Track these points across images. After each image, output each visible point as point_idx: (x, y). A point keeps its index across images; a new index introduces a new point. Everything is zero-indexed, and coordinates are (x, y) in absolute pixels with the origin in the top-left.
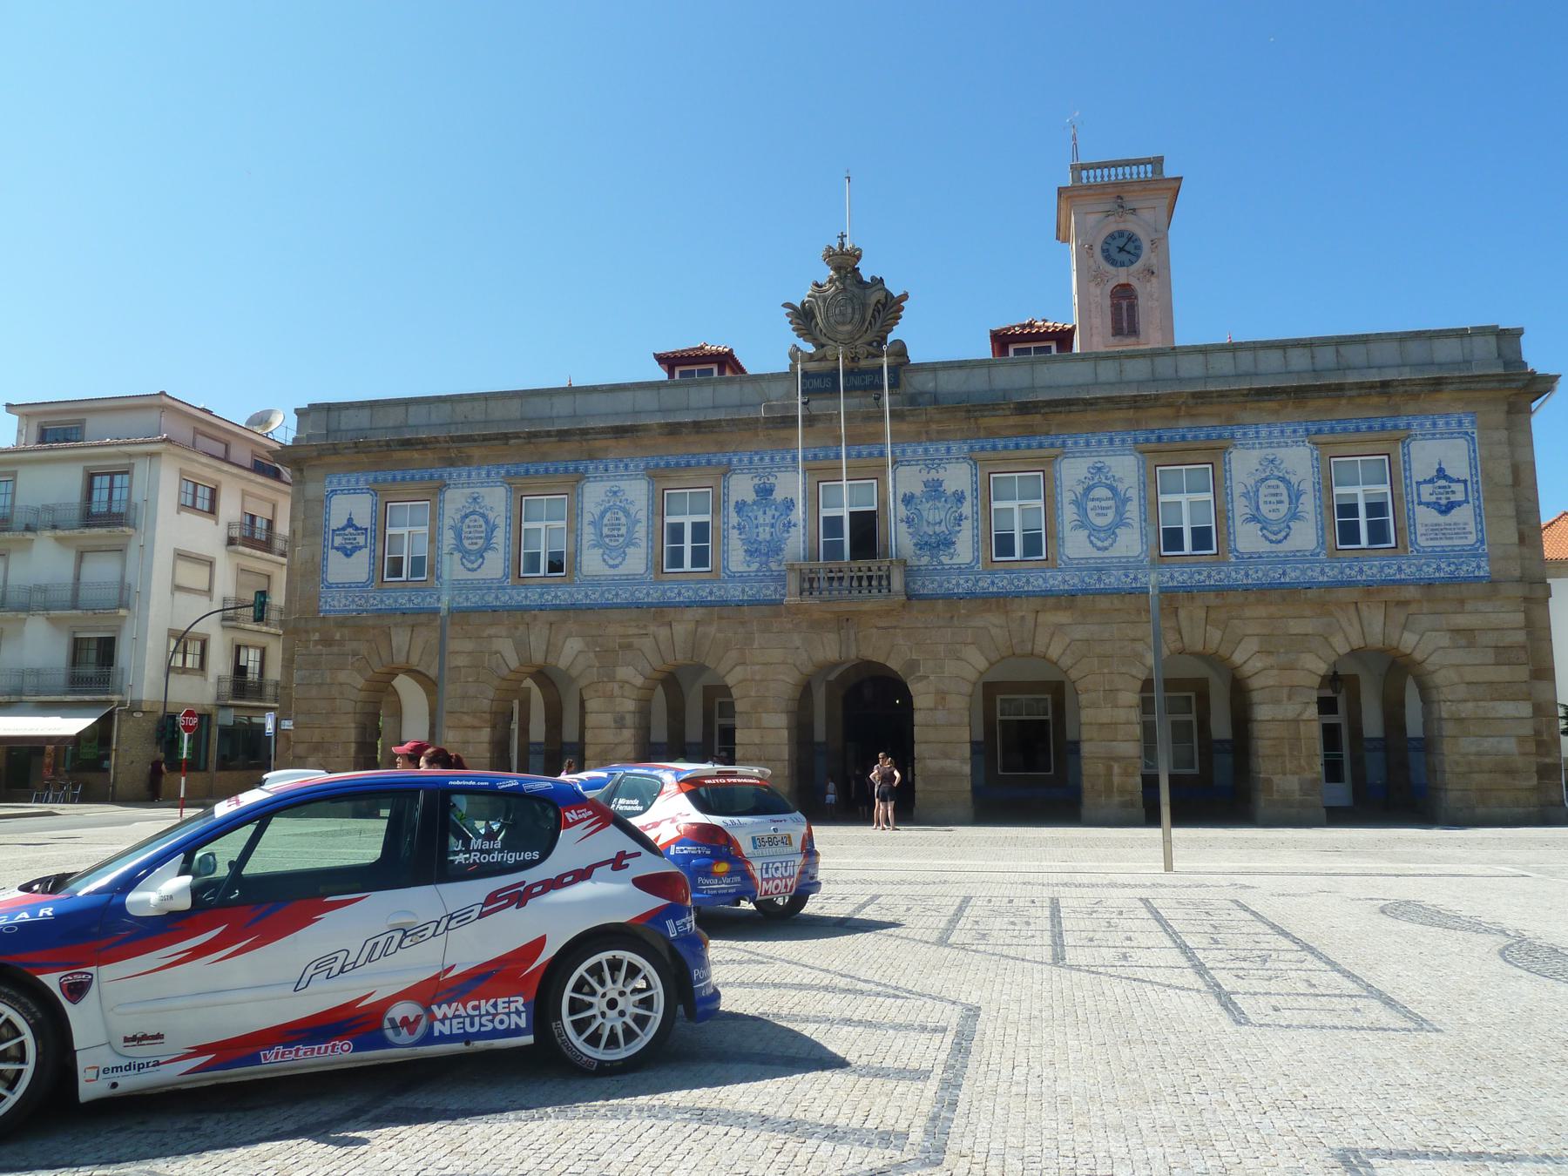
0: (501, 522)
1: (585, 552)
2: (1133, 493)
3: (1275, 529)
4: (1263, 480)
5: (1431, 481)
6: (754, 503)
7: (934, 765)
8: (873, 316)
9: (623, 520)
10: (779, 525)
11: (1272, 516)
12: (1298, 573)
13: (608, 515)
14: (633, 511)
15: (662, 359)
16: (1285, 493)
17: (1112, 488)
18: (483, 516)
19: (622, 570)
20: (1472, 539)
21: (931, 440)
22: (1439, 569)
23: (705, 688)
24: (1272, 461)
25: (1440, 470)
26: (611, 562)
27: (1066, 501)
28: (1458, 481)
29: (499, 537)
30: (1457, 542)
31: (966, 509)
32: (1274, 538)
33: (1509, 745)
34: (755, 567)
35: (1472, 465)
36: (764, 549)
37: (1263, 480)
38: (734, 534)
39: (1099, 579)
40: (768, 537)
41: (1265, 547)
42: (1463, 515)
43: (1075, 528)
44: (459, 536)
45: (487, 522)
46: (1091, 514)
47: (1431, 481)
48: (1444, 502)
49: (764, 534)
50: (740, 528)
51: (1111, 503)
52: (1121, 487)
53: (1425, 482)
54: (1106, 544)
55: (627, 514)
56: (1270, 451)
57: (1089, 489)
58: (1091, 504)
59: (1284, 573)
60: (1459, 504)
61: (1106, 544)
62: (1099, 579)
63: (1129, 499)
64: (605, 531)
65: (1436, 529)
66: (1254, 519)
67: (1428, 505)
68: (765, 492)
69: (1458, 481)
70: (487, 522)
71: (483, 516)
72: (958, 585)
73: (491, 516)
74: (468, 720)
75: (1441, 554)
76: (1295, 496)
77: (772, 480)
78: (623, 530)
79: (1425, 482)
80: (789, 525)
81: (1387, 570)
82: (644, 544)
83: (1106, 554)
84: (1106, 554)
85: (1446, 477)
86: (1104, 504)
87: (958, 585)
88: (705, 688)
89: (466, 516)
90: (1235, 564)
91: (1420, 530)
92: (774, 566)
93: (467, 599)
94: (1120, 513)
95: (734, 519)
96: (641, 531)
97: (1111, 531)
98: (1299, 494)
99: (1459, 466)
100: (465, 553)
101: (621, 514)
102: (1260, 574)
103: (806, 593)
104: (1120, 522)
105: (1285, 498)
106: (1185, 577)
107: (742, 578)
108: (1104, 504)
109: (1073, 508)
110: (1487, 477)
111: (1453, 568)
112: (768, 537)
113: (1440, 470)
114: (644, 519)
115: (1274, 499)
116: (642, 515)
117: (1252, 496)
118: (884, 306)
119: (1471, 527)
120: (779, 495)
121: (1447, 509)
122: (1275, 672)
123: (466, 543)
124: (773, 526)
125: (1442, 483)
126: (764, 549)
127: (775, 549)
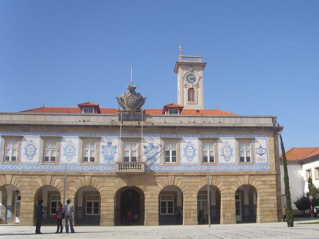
0: (38, 147)
1: (61, 156)
2: (197, 148)
3: (227, 158)
4: (225, 147)
5: (259, 148)
6: (107, 146)
7: (150, 212)
8: (138, 102)
9: (72, 149)
10: (113, 152)
11: (227, 155)
12: (232, 168)
13: (68, 147)
14: (75, 147)
15: (79, 105)
16: (229, 150)
17: (192, 147)
18: (33, 145)
19: (71, 162)
20: (266, 161)
21: (151, 133)
22: (260, 168)
23: (48, 192)
24: (227, 143)
25: (260, 146)
26: (69, 159)
27: (182, 150)
28: (264, 149)
29: (38, 151)
30: (264, 162)
31: (117, 150)
32: (227, 160)
33: (272, 205)
34: (106, 162)
35: (267, 146)
36: (109, 158)
37: (225, 147)
38: (101, 154)
39: (189, 168)
40: (110, 155)
41: (224, 162)
42: (265, 156)
43: (184, 156)
44: (26, 150)
45: (34, 147)
46: (188, 153)
47: (259, 148)
48: (261, 153)
49: (109, 154)
50: (103, 152)
51: (192, 150)
52: (194, 147)
53: (258, 149)
54: (191, 160)
55: (73, 147)
56: (226, 140)
57: (187, 147)
58: (187, 151)
59: (229, 168)
60: (264, 154)
61: (191, 160)
62: (189, 168)
63: (196, 150)
64: (67, 151)
65: (259, 159)
66: (223, 155)
67: (258, 154)
68: (110, 144)
69: (264, 149)
70: (34, 147)
71: (33, 145)
72: (156, 168)
73: (36, 146)
74: (28, 200)
75: (261, 164)
76: (231, 151)
77: (111, 141)
78: (72, 151)
79: (258, 149)
80: (115, 152)
81: (109, 168)
82: (77, 155)
83: (191, 162)
84: (191, 162)
85: (261, 148)
86: (190, 151)
87: (156, 168)
88: (48, 192)
89: (29, 145)
90: (219, 165)
91: (256, 159)
92: (111, 162)
93: (28, 167)
94: (194, 153)
95: (101, 150)
96: (77, 152)
97: (192, 157)
98: (232, 150)
99: (264, 146)
100: (28, 155)
101: (71, 147)
102: (224, 168)
103: (120, 169)
104: (194, 155)
105: (229, 151)
106: (73, 168)
107: (103, 165)
108: (190, 151)
109: (184, 151)
110: (269, 148)
111: (262, 167)
112: (110, 155)
113: (260, 146)
114: (78, 149)
115: (227, 151)
116: (77, 148)
117: (222, 150)
118: (141, 100)
119: (266, 159)
120: (113, 145)
121: (262, 155)
122: (226, 190)
123: (28, 152)
124: (111, 152)
125: (261, 149)
126: (109, 158)
127: (112, 158)
